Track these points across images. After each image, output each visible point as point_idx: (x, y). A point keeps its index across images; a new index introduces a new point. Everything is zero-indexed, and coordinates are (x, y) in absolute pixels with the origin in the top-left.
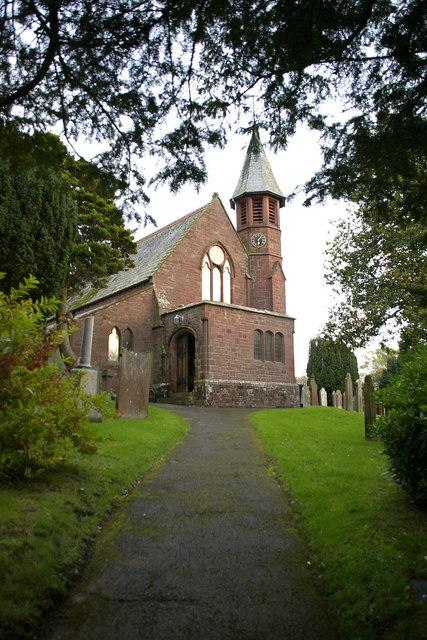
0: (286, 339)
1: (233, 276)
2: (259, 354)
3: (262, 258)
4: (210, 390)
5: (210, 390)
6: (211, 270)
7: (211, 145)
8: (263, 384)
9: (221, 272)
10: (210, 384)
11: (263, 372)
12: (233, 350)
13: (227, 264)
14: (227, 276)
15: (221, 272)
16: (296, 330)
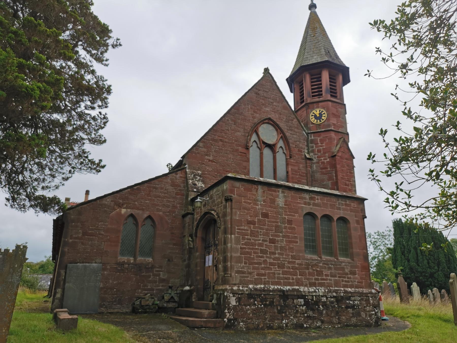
0: (353, 224)
1: (289, 156)
2: (311, 246)
3: (323, 135)
4: (233, 302)
5: (233, 302)
6: (260, 149)
7: (46, 213)
8: (321, 291)
9: (274, 152)
10: (234, 293)
11: (320, 273)
12: (272, 241)
13: (281, 143)
14: (281, 158)
15: (274, 152)
16: (368, 212)
